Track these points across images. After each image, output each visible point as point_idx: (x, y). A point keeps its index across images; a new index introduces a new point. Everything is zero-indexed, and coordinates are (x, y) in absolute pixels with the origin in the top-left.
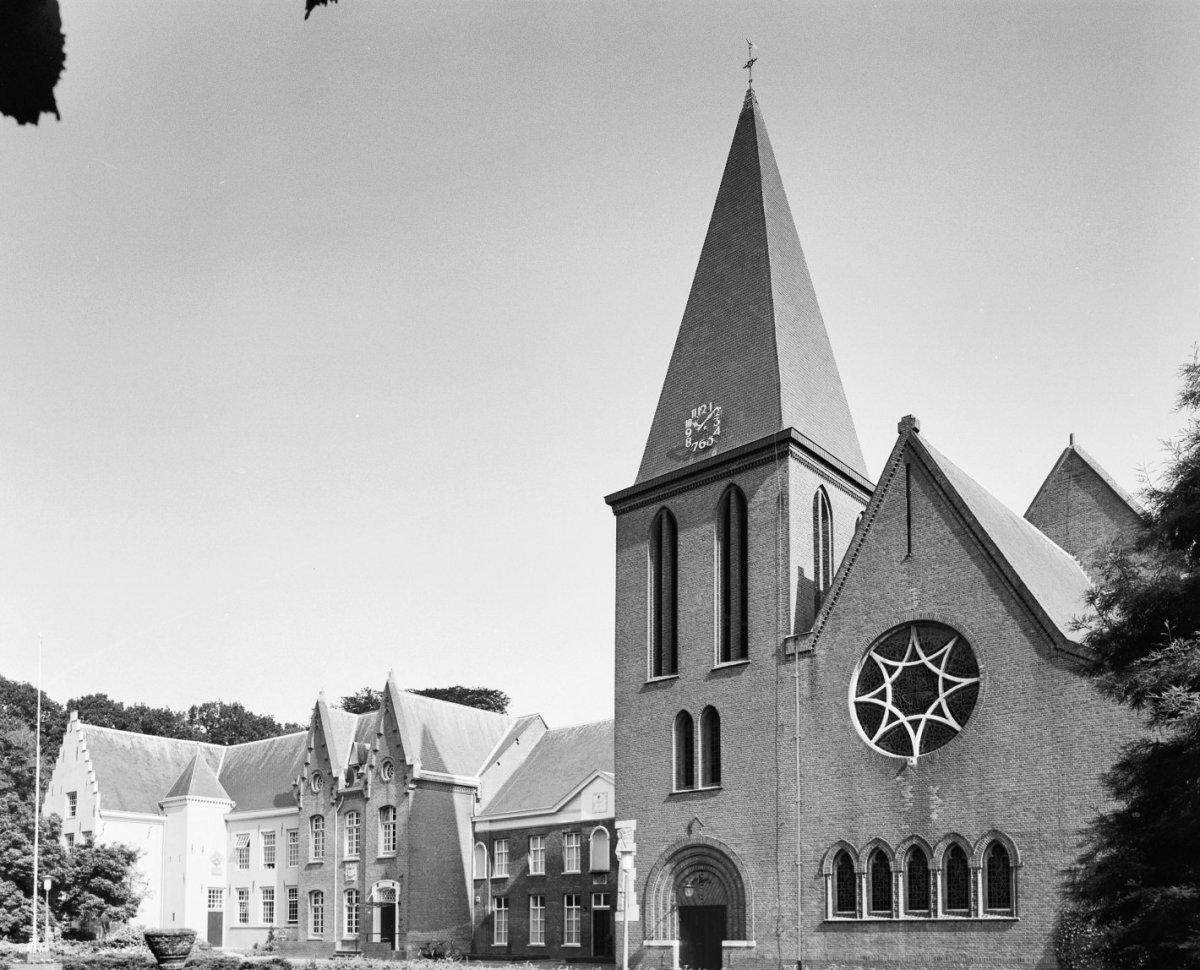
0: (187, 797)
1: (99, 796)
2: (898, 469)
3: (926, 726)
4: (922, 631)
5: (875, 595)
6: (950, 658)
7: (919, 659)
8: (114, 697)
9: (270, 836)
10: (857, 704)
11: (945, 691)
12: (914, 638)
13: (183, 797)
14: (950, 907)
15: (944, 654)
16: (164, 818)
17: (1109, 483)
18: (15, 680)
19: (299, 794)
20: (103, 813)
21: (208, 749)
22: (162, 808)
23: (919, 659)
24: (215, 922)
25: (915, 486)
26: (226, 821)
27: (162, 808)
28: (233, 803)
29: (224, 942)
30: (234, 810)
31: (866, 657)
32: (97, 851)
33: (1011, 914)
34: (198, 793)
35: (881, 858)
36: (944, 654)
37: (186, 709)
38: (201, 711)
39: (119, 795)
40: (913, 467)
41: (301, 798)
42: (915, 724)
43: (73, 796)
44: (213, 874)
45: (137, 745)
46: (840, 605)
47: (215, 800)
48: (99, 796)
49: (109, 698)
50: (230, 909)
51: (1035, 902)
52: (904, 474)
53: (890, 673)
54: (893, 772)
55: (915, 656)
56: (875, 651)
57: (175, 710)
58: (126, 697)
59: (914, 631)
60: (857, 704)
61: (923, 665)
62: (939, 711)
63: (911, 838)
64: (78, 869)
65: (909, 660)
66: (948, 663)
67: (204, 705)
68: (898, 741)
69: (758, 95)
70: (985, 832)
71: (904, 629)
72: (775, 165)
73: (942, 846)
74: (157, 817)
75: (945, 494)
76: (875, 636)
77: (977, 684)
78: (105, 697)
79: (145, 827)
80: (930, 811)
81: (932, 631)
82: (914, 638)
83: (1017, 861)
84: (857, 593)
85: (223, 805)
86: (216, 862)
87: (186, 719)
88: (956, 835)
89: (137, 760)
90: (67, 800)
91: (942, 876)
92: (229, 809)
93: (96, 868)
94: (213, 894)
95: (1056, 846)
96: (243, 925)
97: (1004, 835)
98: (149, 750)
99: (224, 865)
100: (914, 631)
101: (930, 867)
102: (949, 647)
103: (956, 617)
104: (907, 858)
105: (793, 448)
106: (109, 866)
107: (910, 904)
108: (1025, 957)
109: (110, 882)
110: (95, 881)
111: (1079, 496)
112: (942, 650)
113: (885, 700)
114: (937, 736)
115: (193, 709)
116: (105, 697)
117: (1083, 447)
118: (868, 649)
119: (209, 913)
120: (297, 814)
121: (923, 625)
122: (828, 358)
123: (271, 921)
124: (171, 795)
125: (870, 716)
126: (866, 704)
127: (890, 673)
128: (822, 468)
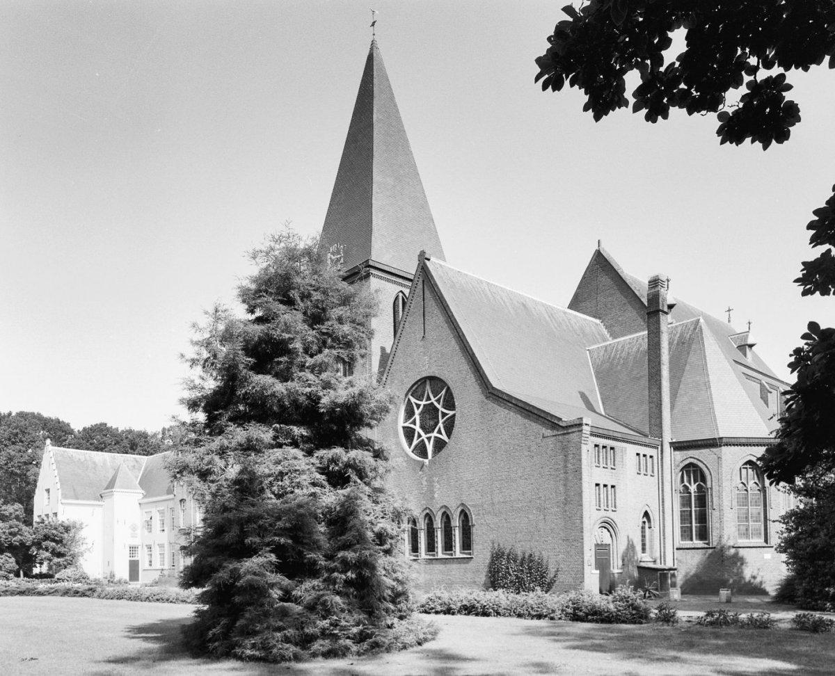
0: (114, 490)
1: (60, 490)
2: (419, 283)
3: (434, 440)
4: (432, 382)
5: (409, 361)
6: (445, 399)
7: (430, 400)
8: (112, 423)
9: (162, 512)
10: (404, 428)
11: (443, 418)
12: (428, 388)
13: (110, 490)
14: (446, 550)
15: (441, 397)
16: (103, 503)
17: (619, 271)
18: (57, 416)
19: (174, 487)
20: (63, 501)
21: (135, 458)
22: (102, 497)
23: (430, 400)
24: (134, 568)
25: (427, 292)
26: (140, 504)
27: (102, 497)
28: (143, 492)
29: (140, 579)
30: (145, 497)
31: (407, 399)
32: (46, 525)
33: (470, 554)
34: (122, 487)
35: (447, 518)
36: (441, 397)
37: (160, 430)
38: (169, 430)
39: (74, 490)
40: (426, 281)
41: (175, 489)
42: (429, 439)
43: (48, 491)
44: (132, 537)
45: (88, 458)
46: (394, 368)
47: (132, 491)
48: (60, 490)
49: (109, 425)
50: (142, 557)
51: (481, 547)
52: (421, 286)
53: (418, 408)
54: (418, 468)
55: (429, 398)
56: (412, 395)
57: (150, 431)
58: (119, 422)
59: (428, 382)
60: (404, 428)
61: (424, 405)
62: (439, 432)
63: (426, 509)
64: (34, 536)
65: (427, 401)
66: (444, 402)
67: (171, 427)
68: (421, 449)
69: (379, 44)
70: (459, 504)
71: (423, 381)
72: (390, 86)
73: (440, 514)
74: (97, 503)
75: (439, 298)
76: (409, 386)
77: (454, 415)
78: (106, 424)
79: (90, 509)
80: (434, 493)
81: (435, 382)
82: (428, 388)
83: (472, 523)
84: (401, 360)
85: (138, 494)
86: (134, 528)
87: (160, 436)
88: (446, 507)
89: (87, 468)
90: (46, 493)
91: (441, 531)
92: (142, 496)
93: (45, 536)
94: (133, 549)
95: (489, 512)
96: (675, 548)
97: (467, 507)
98: (97, 461)
99: (139, 531)
100: (428, 382)
101: (434, 527)
102: (444, 392)
103: (444, 375)
104: (426, 521)
105: (373, 271)
106: (53, 534)
107: (428, 547)
108: (477, 579)
109: (54, 544)
110: (44, 544)
111: (605, 280)
112: (440, 395)
113: (415, 425)
114: (440, 445)
115: (164, 429)
116: (106, 424)
117: (606, 249)
118: (406, 395)
119: (130, 561)
120: (173, 499)
121: (432, 379)
122: (424, 206)
123: (164, 565)
124: (107, 488)
125: (409, 434)
126: (408, 427)
127: (418, 408)
128: (400, 281)
